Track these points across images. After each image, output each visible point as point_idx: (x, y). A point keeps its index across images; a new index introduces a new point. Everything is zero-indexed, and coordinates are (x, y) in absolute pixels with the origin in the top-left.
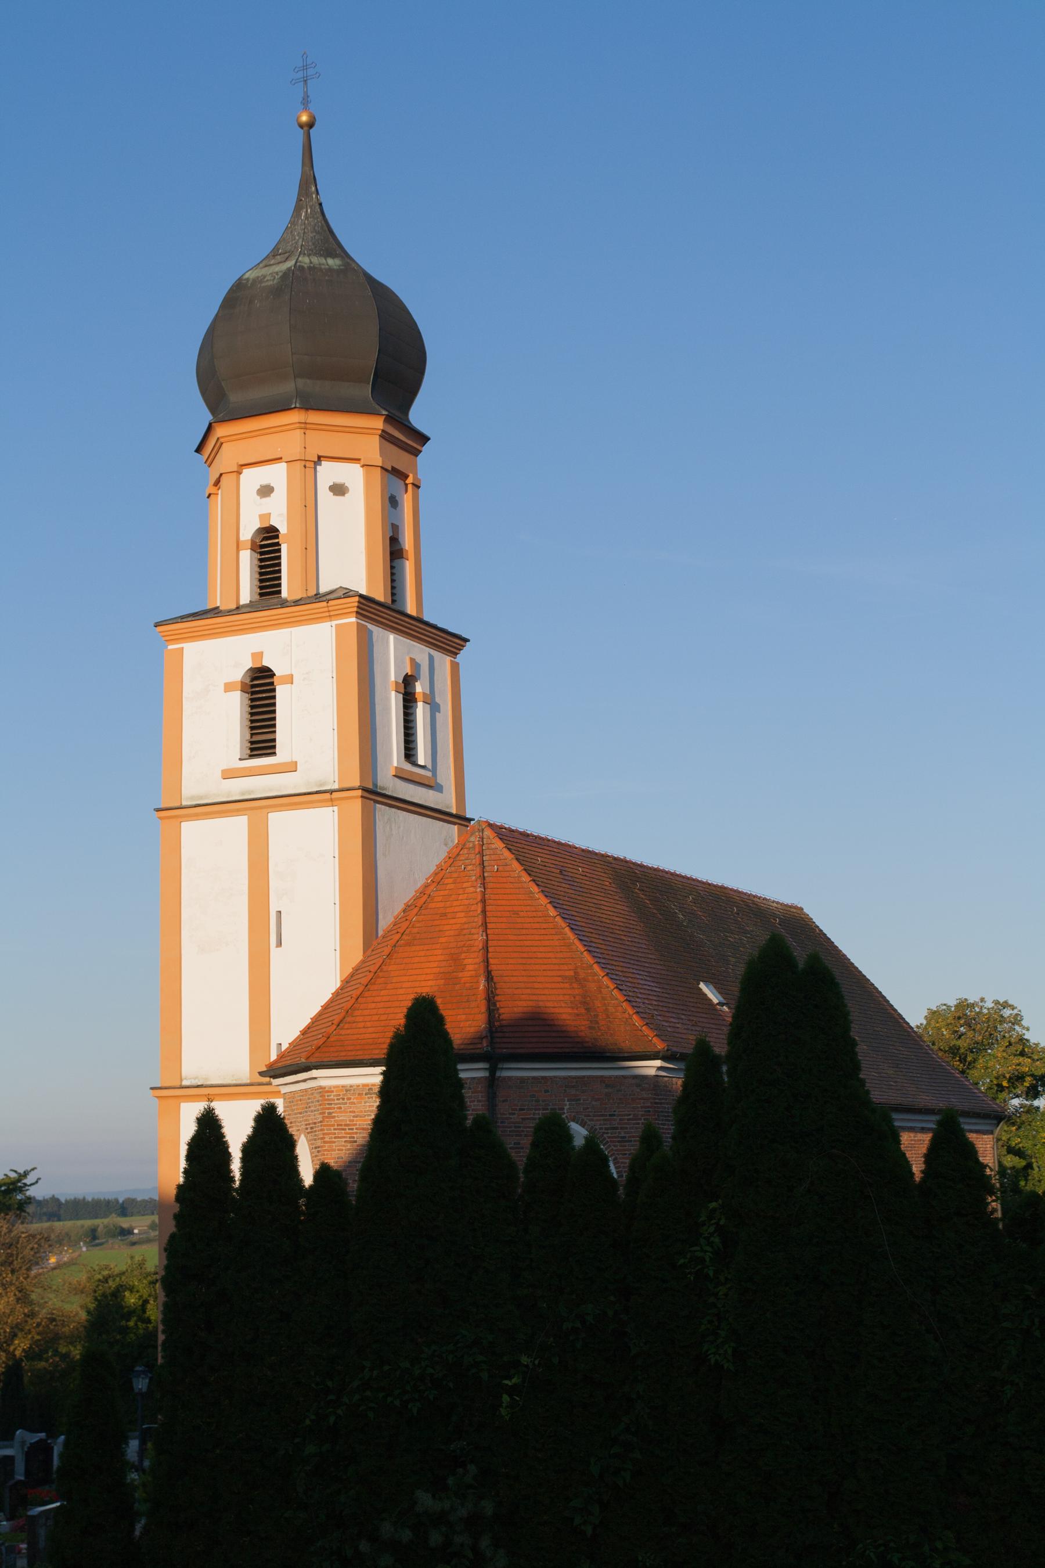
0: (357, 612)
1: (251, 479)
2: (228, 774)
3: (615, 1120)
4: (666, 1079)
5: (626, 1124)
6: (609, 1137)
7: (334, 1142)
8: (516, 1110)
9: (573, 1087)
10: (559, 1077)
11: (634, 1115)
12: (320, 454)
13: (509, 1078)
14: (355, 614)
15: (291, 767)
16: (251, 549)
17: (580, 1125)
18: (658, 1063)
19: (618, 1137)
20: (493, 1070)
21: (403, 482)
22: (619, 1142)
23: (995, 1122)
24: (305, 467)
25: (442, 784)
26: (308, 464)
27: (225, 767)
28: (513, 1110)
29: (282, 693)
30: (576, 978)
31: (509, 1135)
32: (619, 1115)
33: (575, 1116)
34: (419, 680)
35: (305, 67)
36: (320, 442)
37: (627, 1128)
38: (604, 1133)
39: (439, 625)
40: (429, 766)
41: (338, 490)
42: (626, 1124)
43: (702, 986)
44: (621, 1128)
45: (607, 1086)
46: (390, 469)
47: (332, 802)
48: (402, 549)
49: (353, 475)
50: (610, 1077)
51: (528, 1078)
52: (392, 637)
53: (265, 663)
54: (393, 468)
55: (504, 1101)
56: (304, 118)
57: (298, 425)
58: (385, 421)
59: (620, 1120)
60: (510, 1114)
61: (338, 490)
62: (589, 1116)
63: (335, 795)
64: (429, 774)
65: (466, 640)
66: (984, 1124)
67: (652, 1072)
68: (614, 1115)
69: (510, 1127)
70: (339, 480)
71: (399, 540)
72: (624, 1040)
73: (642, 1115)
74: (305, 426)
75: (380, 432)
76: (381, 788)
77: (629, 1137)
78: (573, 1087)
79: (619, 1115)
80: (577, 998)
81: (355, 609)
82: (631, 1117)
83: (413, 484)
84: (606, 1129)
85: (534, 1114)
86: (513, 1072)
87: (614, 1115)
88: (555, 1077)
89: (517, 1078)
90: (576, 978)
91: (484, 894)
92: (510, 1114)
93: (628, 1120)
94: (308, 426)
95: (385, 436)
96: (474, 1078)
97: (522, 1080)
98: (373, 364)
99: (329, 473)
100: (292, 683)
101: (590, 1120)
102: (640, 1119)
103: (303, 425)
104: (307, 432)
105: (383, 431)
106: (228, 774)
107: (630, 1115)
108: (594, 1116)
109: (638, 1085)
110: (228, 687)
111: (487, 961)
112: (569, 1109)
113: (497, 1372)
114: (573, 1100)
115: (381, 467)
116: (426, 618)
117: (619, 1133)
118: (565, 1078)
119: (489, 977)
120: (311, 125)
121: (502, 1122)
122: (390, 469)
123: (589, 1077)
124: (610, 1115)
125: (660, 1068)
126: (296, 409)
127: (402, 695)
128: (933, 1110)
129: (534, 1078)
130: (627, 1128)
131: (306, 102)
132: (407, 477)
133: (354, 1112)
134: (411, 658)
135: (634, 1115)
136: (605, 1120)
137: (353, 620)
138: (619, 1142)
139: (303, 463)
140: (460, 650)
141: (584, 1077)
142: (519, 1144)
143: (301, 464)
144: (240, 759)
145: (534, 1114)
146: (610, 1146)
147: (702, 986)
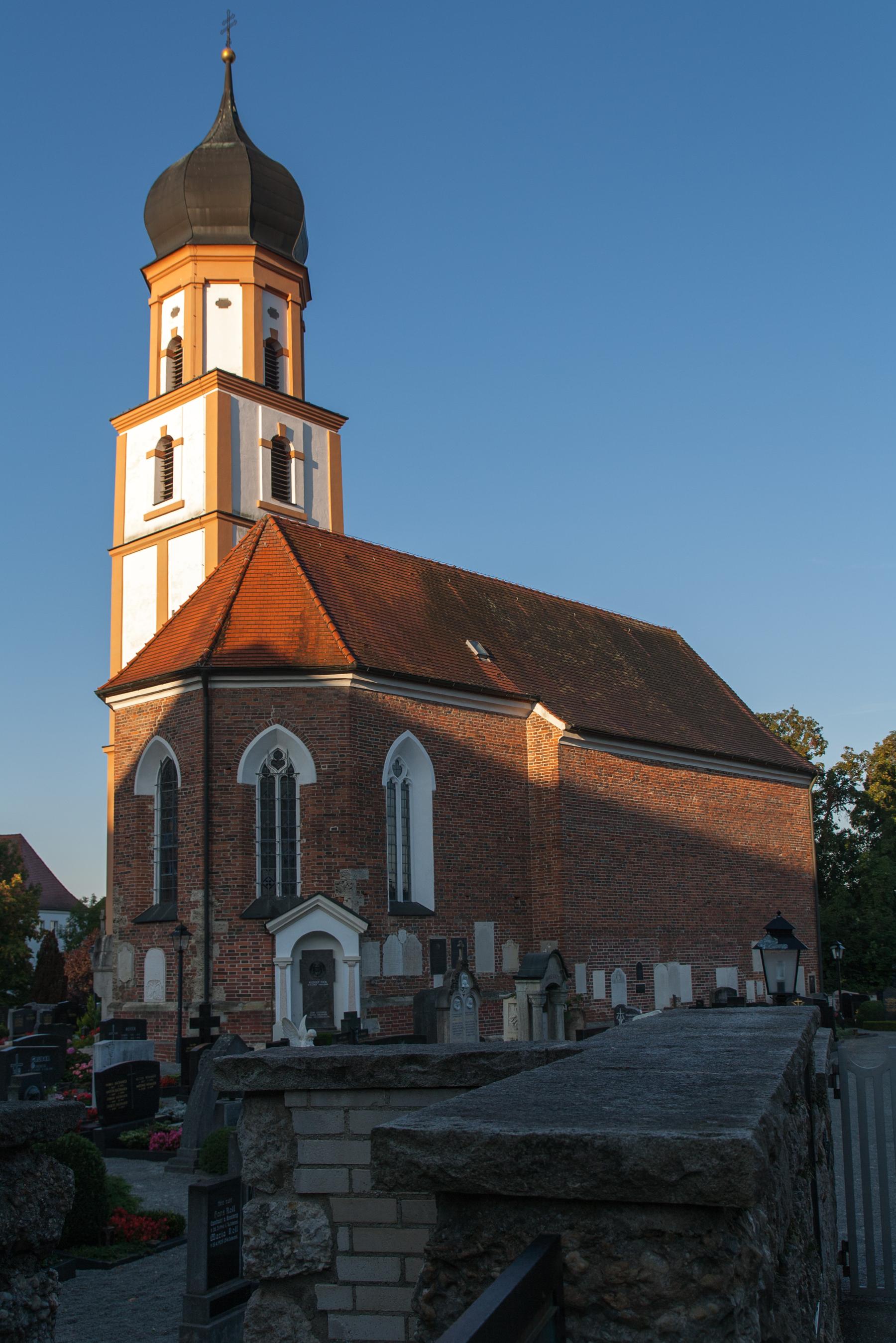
0: (219, 384)
1: (169, 304)
2: (148, 518)
3: (315, 722)
4: (368, 692)
5: (325, 725)
6: (309, 736)
7: (120, 752)
8: (229, 714)
9: (279, 696)
10: (267, 689)
11: (331, 718)
12: (207, 278)
13: (224, 689)
14: (217, 385)
15: (181, 505)
16: (167, 356)
17: (284, 726)
18: (350, 676)
19: (315, 736)
20: (205, 682)
21: (284, 301)
22: (317, 739)
23: (809, 778)
24: (195, 288)
25: (318, 520)
26: (198, 286)
27: (145, 513)
28: (226, 714)
29: (177, 451)
30: (302, 617)
31: (222, 734)
32: (317, 719)
33: (279, 720)
34: (292, 441)
35: (228, 20)
36: (206, 270)
37: (324, 729)
38: (304, 733)
39: (324, 408)
40: (302, 504)
41: (224, 304)
42: (325, 725)
43: (468, 643)
44: (320, 729)
45: (308, 696)
46: (264, 286)
47: (201, 526)
48: (282, 349)
49: (234, 293)
50: (311, 688)
51: (240, 689)
52: (260, 407)
53: (168, 434)
54: (267, 285)
55: (219, 708)
56: (225, 54)
57: (190, 258)
58: (257, 250)
59: (319, 722)
60: (224, 718)
61: (224, 304)
62: (292, 719)
63: (203, 519)
64: (302, 511)
65: (346, 419)
66: (800, 779)
67: (348, 684)
68: (314, 718)
69: (224, 728)
70: (223, 297)
71: (279, 340)
72: (323, 658)
73: (339, 719)
74: (195, 259)
75: (253, 259)
76: (243, 514)
77: (327, 736)
78: (279, 696)
79: (317, 719)
80: (296, 630)
81: (216, 381)
82: (329, 720)
83: (291, 301)
84: (306, 729)
85: (245, 718)
86: (224, 684)
87: (314, 718)
88: (264, 688)
89: (231, 689)
90: (302, 617)
91: (248, 563)
92: (224, 718)
93: (326, 722)
94: (198, 258)
95: (257, 261)
96: (197, 690)
97: (235, 691)
98: (247, 210)
99: (215, 292)
100: (182, 444)
101: (293, 723)
102: (337, 722)
103: (193, 258)
104: (198, 263)
105: (256, 258)
106: (148, 518)
107: (328, 718)
108: (296, 719)
109: (336, 695)
110: (148, 456)
111: (230, 606)
112: (275, 713)
113: (18, 877)
114: (279, 707)
115: (255, 284)
116: (306, 400)
117: (318, 732)
118: (272, 689)
119: (227, 616)
120: (231, 59)
121: (216, 724)
122: (264, 286)
123: (293, 688)
124: (310, 719)
125: (353, 680)
126: (187, 246)
127: (270, 450)
128: (693, 750)
129: (245, 689)
130: (324, 729)
131: (228, 44)
132: (287, 296)
133: (131, 727)
134: (281, 425)
135: (331, 718)
136: (366, 742)
137: (217, 389)
138: (317, 739)
139: (193, 285)
140: (341, 425)
141: (288, 688)
142: (231, 741)
143: (190, 287)
144: (154, 505)
145: (245, 718)
146: (310, 743)
147: (468, 643)
